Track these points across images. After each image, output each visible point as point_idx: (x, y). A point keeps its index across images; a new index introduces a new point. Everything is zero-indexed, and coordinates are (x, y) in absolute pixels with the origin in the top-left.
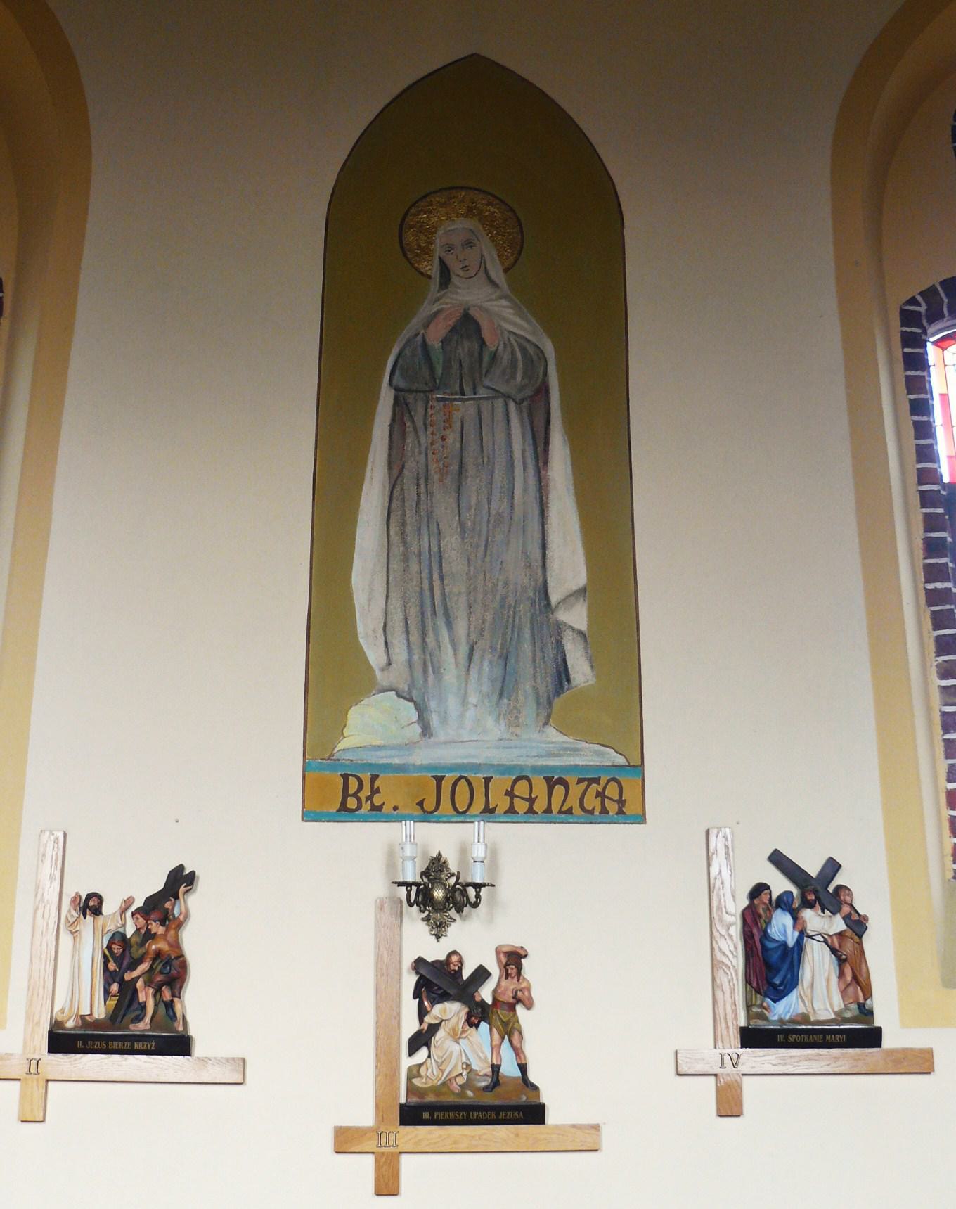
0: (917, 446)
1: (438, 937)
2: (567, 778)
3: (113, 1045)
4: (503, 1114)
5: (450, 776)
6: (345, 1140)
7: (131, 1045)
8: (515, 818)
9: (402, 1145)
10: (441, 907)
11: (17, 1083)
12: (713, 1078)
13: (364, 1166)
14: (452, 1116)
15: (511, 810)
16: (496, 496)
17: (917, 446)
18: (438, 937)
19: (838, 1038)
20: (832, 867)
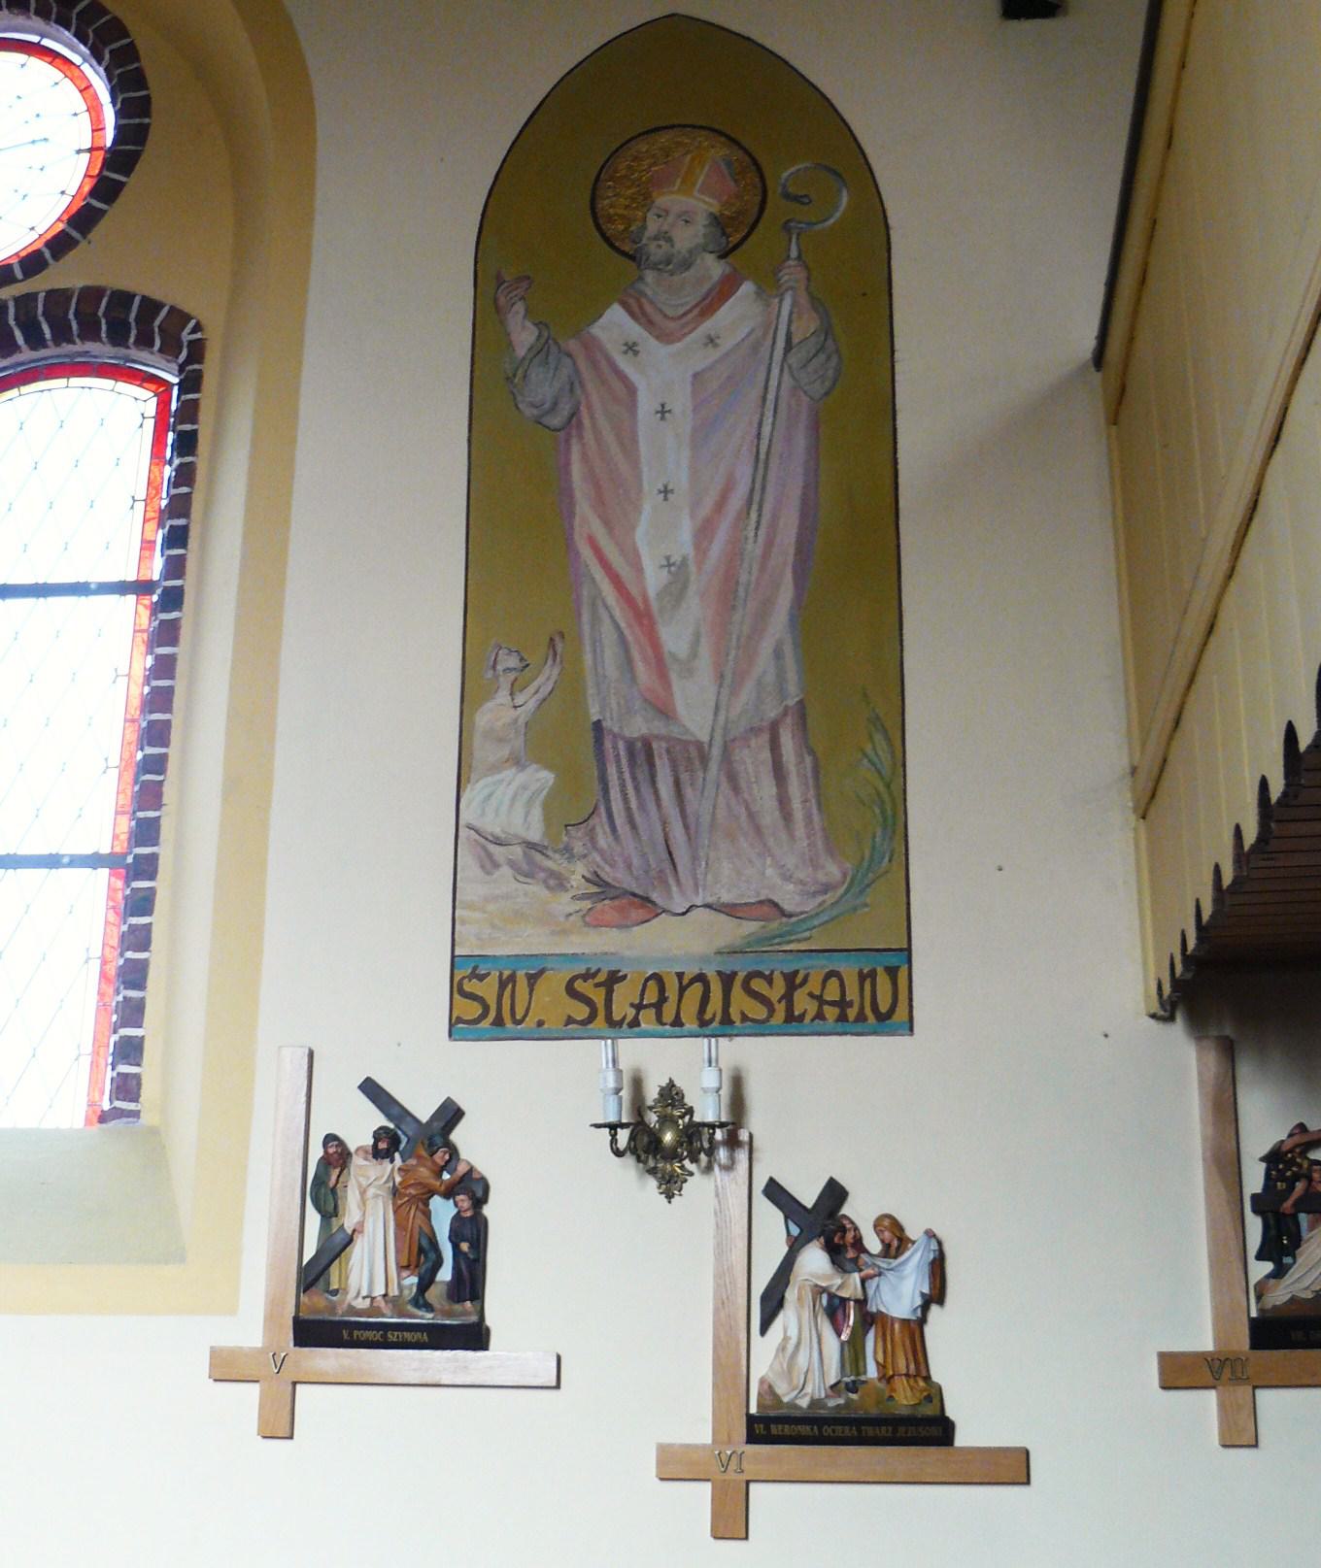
0: (172, 678)
1: (670, 1197)
2: (842, 968)
3: (392, 1337)
4: (902, 1430)
5: (485, 1024)
6: (675, 1466)
7: (440, 1338)
8: (848, 1027)
9: (750, 1470)
10: (672, 1155)
11: (257, 1386)
12: (299, 1387)
13: (699, 1496)
14: (924, 1433)
15: (820, 1016)
16: (640, 667)
17: (172, 678)
18: (670, 1197)
19: (369, 1335)
20: (450, 1115)
